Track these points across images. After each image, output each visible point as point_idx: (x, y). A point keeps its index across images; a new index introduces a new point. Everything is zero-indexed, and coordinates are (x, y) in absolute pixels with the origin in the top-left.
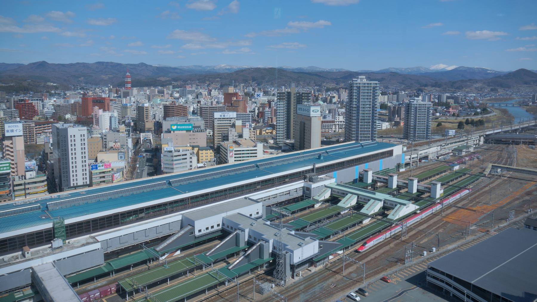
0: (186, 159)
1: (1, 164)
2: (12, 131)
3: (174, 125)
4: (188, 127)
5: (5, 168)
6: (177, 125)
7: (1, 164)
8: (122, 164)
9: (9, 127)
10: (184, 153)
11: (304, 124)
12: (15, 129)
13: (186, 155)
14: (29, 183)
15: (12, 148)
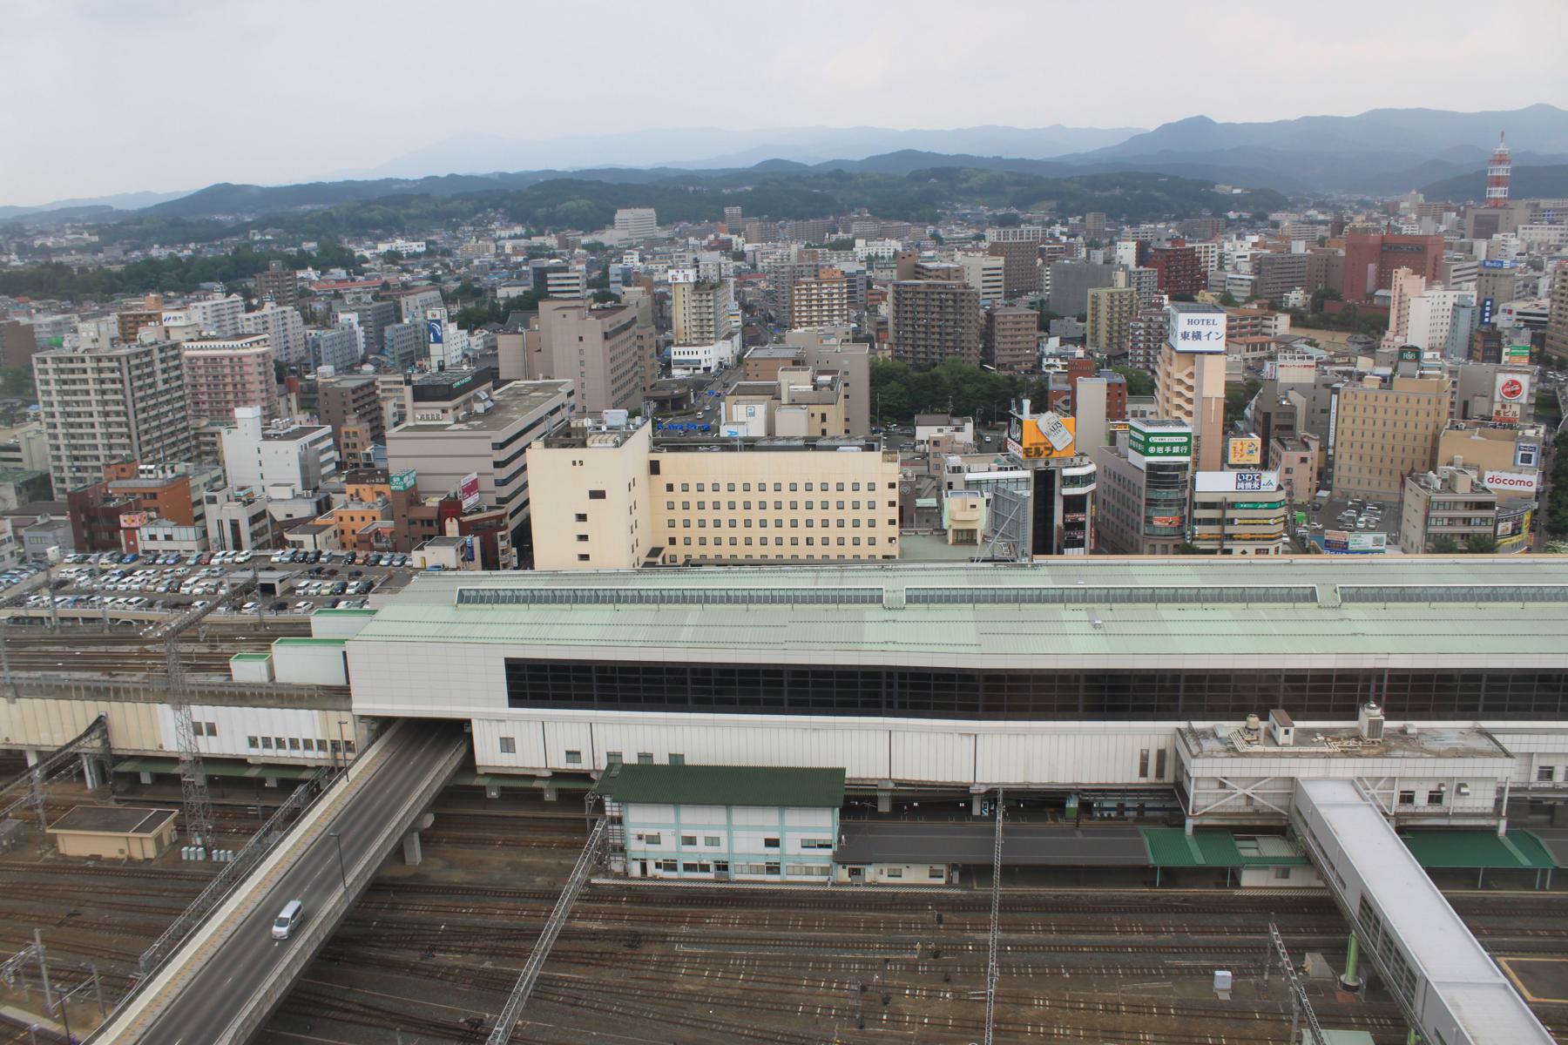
2: (1197, 336)
5: (1176, 449)
8: (1529, 481)
9: (1190, 322)
11: (1470, 356)
12: (1204, 329)
15: (1190, 388)
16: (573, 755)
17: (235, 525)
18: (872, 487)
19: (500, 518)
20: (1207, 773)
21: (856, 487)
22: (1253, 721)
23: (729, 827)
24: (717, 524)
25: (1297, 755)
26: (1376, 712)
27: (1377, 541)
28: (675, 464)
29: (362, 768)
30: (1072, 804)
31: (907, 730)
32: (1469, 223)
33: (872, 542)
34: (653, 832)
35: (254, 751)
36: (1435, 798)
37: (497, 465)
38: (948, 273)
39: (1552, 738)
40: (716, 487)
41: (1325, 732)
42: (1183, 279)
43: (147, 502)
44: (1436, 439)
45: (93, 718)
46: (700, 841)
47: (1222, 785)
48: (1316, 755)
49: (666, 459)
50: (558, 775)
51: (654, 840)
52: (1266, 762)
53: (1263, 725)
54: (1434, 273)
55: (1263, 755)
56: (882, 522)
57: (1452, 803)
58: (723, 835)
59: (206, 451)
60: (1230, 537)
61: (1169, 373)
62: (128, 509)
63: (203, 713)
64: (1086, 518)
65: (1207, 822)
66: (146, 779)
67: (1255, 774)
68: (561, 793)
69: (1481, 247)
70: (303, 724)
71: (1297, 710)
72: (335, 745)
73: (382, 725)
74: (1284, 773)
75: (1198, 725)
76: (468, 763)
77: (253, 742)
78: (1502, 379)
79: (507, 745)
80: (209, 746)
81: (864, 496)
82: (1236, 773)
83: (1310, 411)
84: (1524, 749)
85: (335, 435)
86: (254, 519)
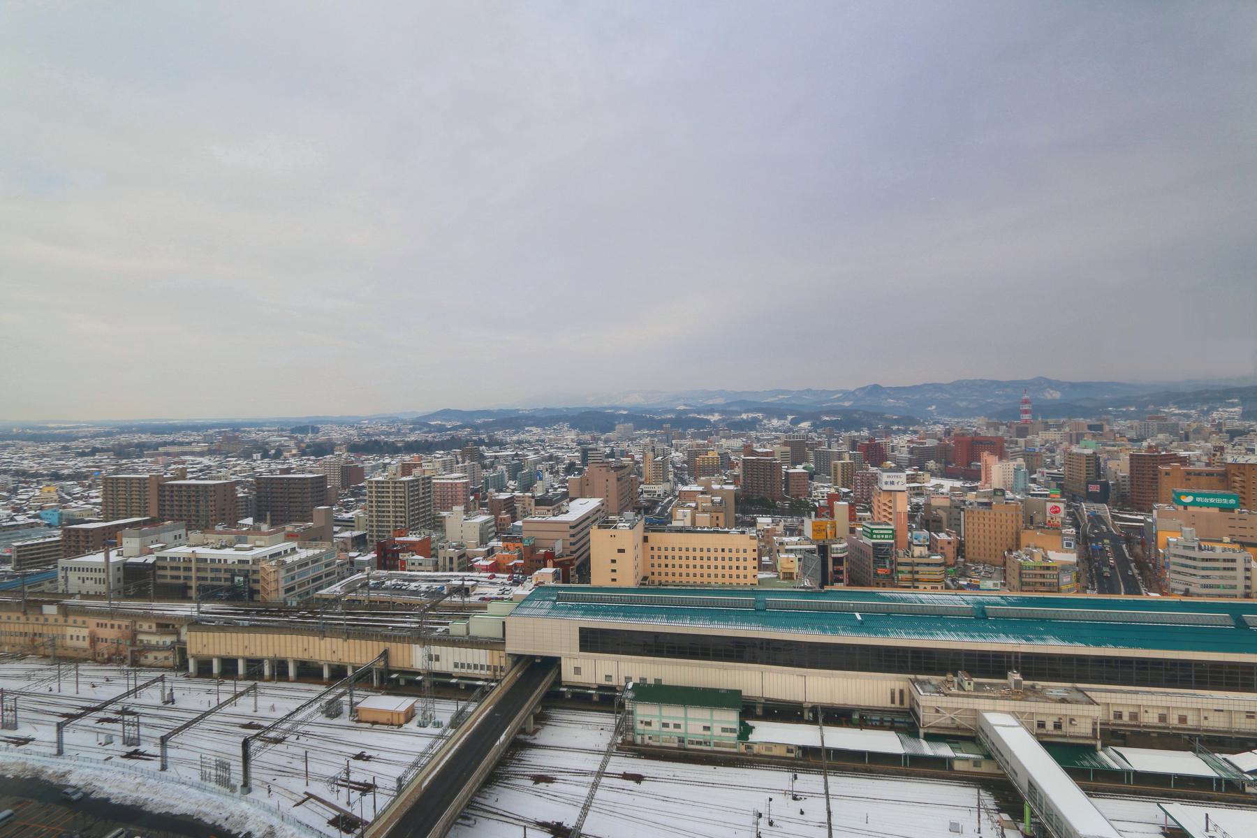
0: (1233, 569)
1: (5, 677)
2: (892, 483)
3: (1187, 495)
4: (1225, 501)
6: (1195, 496)
7: (5, 677)
8: (1072, 558)
10: (1230, 555)
12: (896, 480)
13: (1234, 561)
14: (918, 564)
16: (608, 677)
17: (451, 559)
18: (745, 551)
19: (571, 560)
20: (929, 704)
21: (666, 549)
22: (950, 676)
23: (686, 719)
24: (688, 566)
25: (977, 697)
26: (1018, 677)
27: (995, 585)
28: (657, 538)
29: (508, 680)
30: (856, 717)
31: (771, 671)
32: (1013, 430)
33: (745, 577)
34: (648, 720)
35: (456, 670)
36: (1058, 726)
37: (573, 536)
38: (767, 454)
39: (1118, 695)
40: (673, 549)
41: (990, 685)
42: (875, 454)
43: (411, 547)
44: (1018, 534)
45: (382, 650)
46: (671, 726)
47: (937, 711)
48: (987, 697)
49: (651, 535)
50: (600, 688)
51: (649, 724)
52: (960, 699)
53: (955, 680)
54: (1002, 455)
55: (958, 696)
56: (750, 568)
57: (1067, 729)
58: (682, 723)
59: (438, 524)
60: (917, 580)
61: (879, 501)
62: (403, 551)
63: (435, 650)
64: (844, 568)
65: (931, 731)
66: (402, 682)
67: (955, 706)
68: (601, 696)
69: (1021, 441)
70: (480, 657)
71: (972, 672)
72: (495, 669)
73: (518, 659)
74: (971, 707)
75: (920, 677)
76: (558, 681)
77: (456, 665)
78: (1049, 505)
79: (577, 670)
80: (436, 667)
81: (741, 555)
82: (944, 705)
83: (949, 519)
84: (1104, 701)
85: (496, 519)
86: (459, 557)
